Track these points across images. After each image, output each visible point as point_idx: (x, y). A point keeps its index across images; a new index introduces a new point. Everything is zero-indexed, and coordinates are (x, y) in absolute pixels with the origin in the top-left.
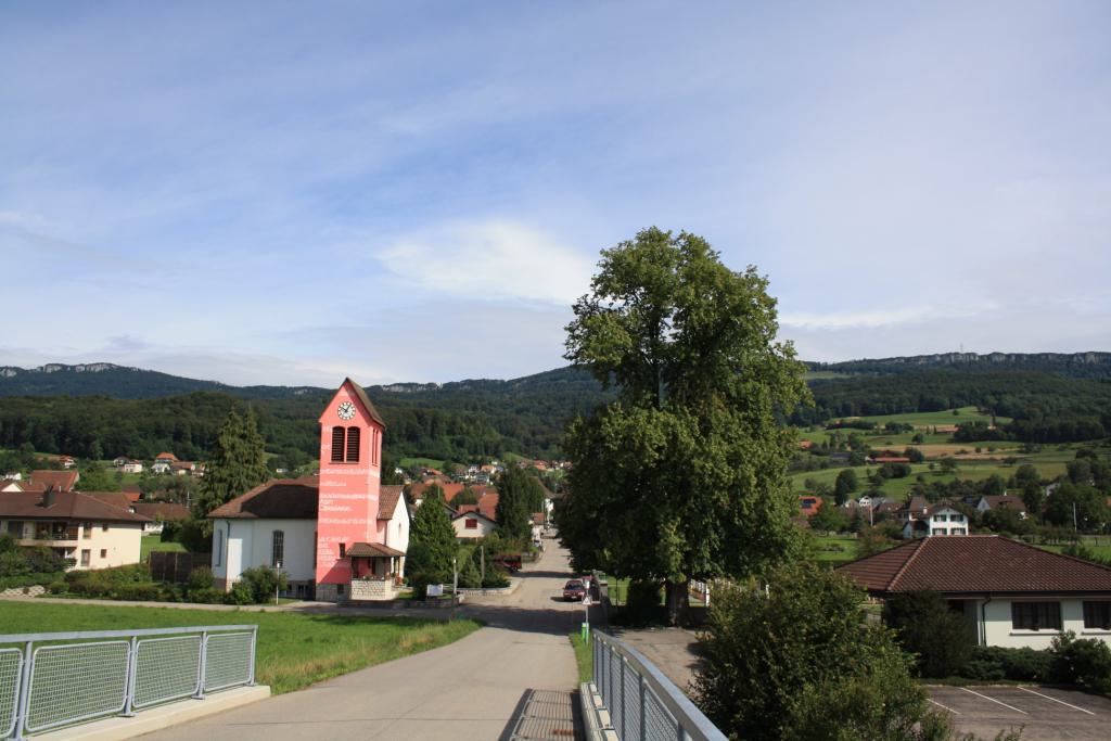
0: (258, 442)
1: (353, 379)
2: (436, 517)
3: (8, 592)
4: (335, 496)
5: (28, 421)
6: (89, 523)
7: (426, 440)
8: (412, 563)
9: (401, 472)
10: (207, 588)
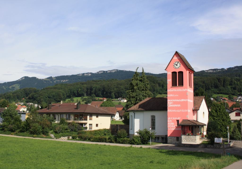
0: (147, 82)
1: (179, 52)
2: (220, 109)
3: (62, 138)
4: (174, 101)
5: (93, 88)
6: (91, 115)
7: (222, 88)
8: (210, 128)
9: (213, 99)
10: (124, 137)
